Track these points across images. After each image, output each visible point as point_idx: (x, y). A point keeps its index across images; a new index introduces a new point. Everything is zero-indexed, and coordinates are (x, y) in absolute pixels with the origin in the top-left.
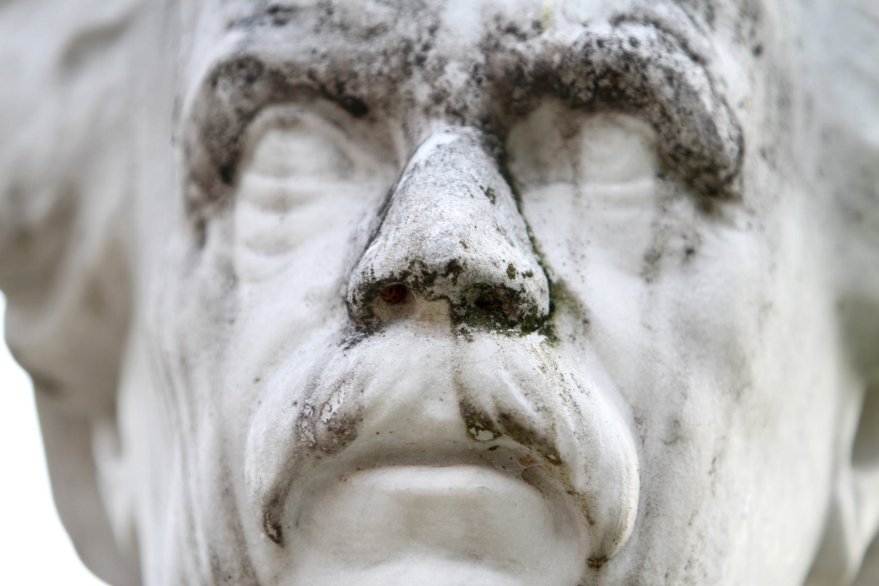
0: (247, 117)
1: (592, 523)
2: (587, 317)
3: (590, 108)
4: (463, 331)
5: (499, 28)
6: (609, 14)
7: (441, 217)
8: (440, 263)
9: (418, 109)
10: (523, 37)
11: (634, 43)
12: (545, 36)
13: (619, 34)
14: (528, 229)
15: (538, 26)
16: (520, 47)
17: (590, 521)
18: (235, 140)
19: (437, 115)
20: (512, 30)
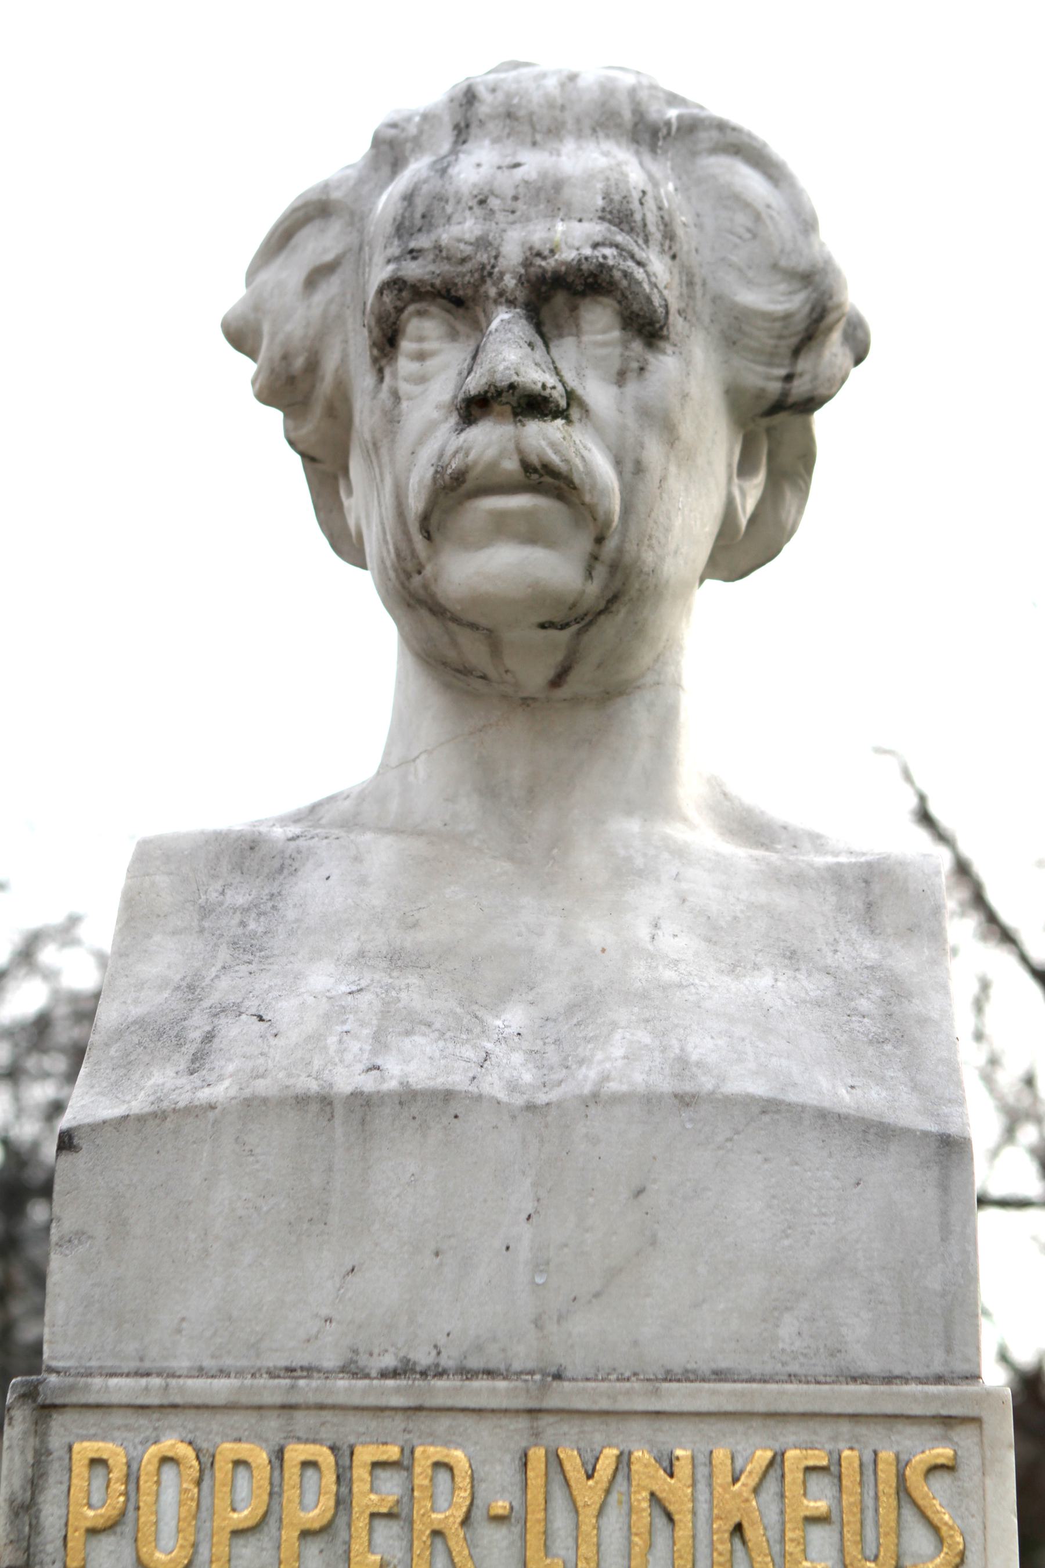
1: (595, 519)
6: (590, 242)
10: (544, 258)
11: (605, 257)
12: (557, 257)
13: (596, 253)
15: (552, 252)
16: (543, 263)
18: (394, 323)
20: (539, 254)
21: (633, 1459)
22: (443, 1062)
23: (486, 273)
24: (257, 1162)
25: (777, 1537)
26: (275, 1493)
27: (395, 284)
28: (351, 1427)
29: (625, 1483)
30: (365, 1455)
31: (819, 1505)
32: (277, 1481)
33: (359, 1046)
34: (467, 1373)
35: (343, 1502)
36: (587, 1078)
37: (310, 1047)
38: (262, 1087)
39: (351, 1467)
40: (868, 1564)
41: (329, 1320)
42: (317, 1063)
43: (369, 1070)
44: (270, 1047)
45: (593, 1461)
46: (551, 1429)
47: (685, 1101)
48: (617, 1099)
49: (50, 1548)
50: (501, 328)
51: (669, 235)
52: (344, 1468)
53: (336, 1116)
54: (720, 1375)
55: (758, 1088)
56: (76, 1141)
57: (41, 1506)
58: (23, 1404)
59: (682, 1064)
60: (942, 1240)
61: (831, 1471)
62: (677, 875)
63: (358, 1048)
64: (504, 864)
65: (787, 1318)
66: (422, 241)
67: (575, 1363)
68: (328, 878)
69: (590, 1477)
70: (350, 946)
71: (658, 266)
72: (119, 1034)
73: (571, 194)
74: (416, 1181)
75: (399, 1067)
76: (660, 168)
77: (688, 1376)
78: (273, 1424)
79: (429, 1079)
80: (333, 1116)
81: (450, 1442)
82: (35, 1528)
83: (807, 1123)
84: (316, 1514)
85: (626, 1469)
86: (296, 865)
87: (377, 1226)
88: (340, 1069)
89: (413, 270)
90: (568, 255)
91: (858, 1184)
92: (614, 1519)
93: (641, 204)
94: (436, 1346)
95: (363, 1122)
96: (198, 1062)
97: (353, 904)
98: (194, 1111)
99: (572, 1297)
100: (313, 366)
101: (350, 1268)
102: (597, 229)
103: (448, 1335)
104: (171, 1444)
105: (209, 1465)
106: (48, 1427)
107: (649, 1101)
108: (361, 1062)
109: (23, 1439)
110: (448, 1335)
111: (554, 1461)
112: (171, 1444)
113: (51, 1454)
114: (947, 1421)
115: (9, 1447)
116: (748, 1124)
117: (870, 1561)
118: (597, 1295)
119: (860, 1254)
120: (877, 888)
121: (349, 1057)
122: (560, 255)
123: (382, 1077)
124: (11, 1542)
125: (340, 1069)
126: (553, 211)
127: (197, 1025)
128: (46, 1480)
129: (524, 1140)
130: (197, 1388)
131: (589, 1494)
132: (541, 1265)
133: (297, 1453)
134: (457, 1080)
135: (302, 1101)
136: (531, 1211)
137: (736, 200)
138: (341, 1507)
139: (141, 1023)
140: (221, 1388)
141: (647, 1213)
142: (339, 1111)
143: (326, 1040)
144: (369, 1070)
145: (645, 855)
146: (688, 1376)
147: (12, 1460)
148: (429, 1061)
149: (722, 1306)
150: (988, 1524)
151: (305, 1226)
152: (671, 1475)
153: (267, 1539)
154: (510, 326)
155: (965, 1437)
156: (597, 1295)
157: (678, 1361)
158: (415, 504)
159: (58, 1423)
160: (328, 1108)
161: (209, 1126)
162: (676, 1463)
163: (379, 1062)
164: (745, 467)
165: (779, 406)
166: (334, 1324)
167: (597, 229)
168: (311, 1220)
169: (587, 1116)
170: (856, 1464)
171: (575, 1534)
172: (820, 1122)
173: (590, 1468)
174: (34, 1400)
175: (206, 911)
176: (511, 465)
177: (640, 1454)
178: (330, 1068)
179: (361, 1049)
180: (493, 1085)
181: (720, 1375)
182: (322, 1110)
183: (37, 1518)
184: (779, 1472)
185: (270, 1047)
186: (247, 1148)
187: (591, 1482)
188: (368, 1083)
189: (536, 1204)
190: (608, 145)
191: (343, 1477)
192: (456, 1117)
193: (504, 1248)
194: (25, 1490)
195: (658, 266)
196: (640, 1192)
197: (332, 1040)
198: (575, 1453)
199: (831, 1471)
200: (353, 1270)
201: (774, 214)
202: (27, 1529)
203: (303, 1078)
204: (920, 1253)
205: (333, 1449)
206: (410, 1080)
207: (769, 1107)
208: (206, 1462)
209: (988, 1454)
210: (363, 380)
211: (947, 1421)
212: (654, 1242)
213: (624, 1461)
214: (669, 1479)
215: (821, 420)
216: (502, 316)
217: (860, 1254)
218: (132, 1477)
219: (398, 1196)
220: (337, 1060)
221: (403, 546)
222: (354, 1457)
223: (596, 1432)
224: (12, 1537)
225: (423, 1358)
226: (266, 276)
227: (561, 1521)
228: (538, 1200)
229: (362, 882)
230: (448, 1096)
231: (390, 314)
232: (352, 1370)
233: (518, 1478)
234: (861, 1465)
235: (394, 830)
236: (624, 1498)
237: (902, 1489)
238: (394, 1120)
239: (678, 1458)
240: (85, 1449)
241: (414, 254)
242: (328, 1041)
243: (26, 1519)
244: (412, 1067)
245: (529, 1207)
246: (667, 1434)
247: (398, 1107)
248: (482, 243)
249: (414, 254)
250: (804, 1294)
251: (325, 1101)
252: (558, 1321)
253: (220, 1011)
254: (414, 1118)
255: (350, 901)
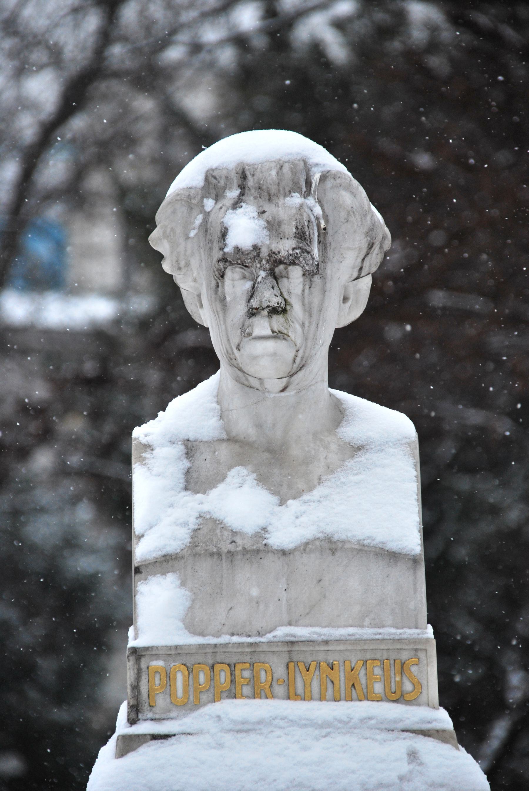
0: (225, 268)
1: (296, 346)
2: (292, 305)
3: (290, 265)
4: (270, 315)
5: (271, 252)
6: (292, 248)
7: (265, 297)
8: (266, 453)
9: (258, 268)
10: (276, 254)
11: (297, 254)
12: (280, 254)
13: (294, 252)
14: (280, 290)
15: (279, 252)
16: (276, 256)
17: (236, 732)
18: (224, 272)
19: (261, 269)
20: (274, 253)
21: (321, 665)
22: (255, 539)
24: (199, 575)
25: (365, 687)
29: (319, 672)
32: (212, 676)
33: (227, 533)
37: (211, 534)
39: (235, 671)
40: (393, 694)
41: (224, 624)
42: (215, 540)
43: (232, 543)
44: (198, 534)
45: (308, 666)
49: (144, 699)
50: (262, 281)
52: (232, 671)
53: (223, 559)
56: (141, 570)
57: (140, 686)
58: (132, 655)
60: (414, 593)
62: (326, 456)
64: (266, 454)
65: (367, 619)
68: (205, 460)
69: (308, 671)
74: (249, 579)
75: (241, 541)
79: (251, 546)
80: (222, 560)
82: (139, 693)
83: (371, 557)
85: (319, 668)
86: (193, 452)
87: (238, 594)
88: (222, 543)
91: (388, 576)
93: (308, 227)
94: (258, 632)
95: (232, 561)
97: (216, 472)
99: (300, 615)
101: (230, 608)
103: (262, 628)
105: (191, 672)
106: (140, 662)
108: (229, 539)
109: (133, 666)
110: (262, 628)
113: (142, 670)
115: (129, 668)
116: (353, 558)
117: (393, 693)
118: (308, 614)
119: (389, 599)
121: (225, 538)
122: (281, 254)
123: (236, 545)
124: (132, 697)
125: (222, 543)
126: (278, 235)
128: (141, 678)
129: (283, 565)
136: (286, 588)
138: (232, 683)
141: (322, 588)
142: (224, 557)
143: (216, 531)
144: (232, 543)
145: (315, 449)
147: (130, 673)
148: (250, 539)
149: (346, 616)
150: (429, 681)
151: (216, 595)
152: (332, 669)
153: (210, 693)
154: (266, 280)
156: (308, 614)
160: (220, 557)
161: (183, 564)
162: (334, 666)
163: (234, 539)
166: (226, 626)
168: (217, 593)
169: (302, 557)
170: (389, 664)
171: (304, 688)
172: (376, 556)
173: (308, 668)
174: (136, 654)
177: (323, 663)
178: (219, 542)
179: (228, 534)
182: (218, 558)
183: (139, 690)
184: (365, 667)
185: (198, 534)
186: (196, 571)
187: (308, 673)
189: (287, 586)
192: (261, 558)
193: (278, 600)
194: (135, 682)
196: (320, 581)
197: (218, 531)
198: (303, 664)
200: (231, 609)
201: (354, 210)
202: (137, 693)
203: (211, 546)
204: (407, 597)
205: (229, 665)
206: (245, 546)
209: (429, 660)
212: (325, 597)
214: (332, 671)
217: (389, 599)
219: (244, 584)
220: (221, 539)
221: (228, 346)
222: (236, 668)
224: (132, 696)
228: (288, 585)
229: (218, 462)
231: (222, 269)
233: (286, 672)
234: (390, 664)
236: (318, 677)
238: (241, 560)
239: (334, 664)
242: (217, 532)
243: (136, 690)
244: (245, 541)
245: (285, 587)
247: (242, 556)
250: (372, 611)
252: (296, 622)
254: (248, 559)
255: (215, 471)
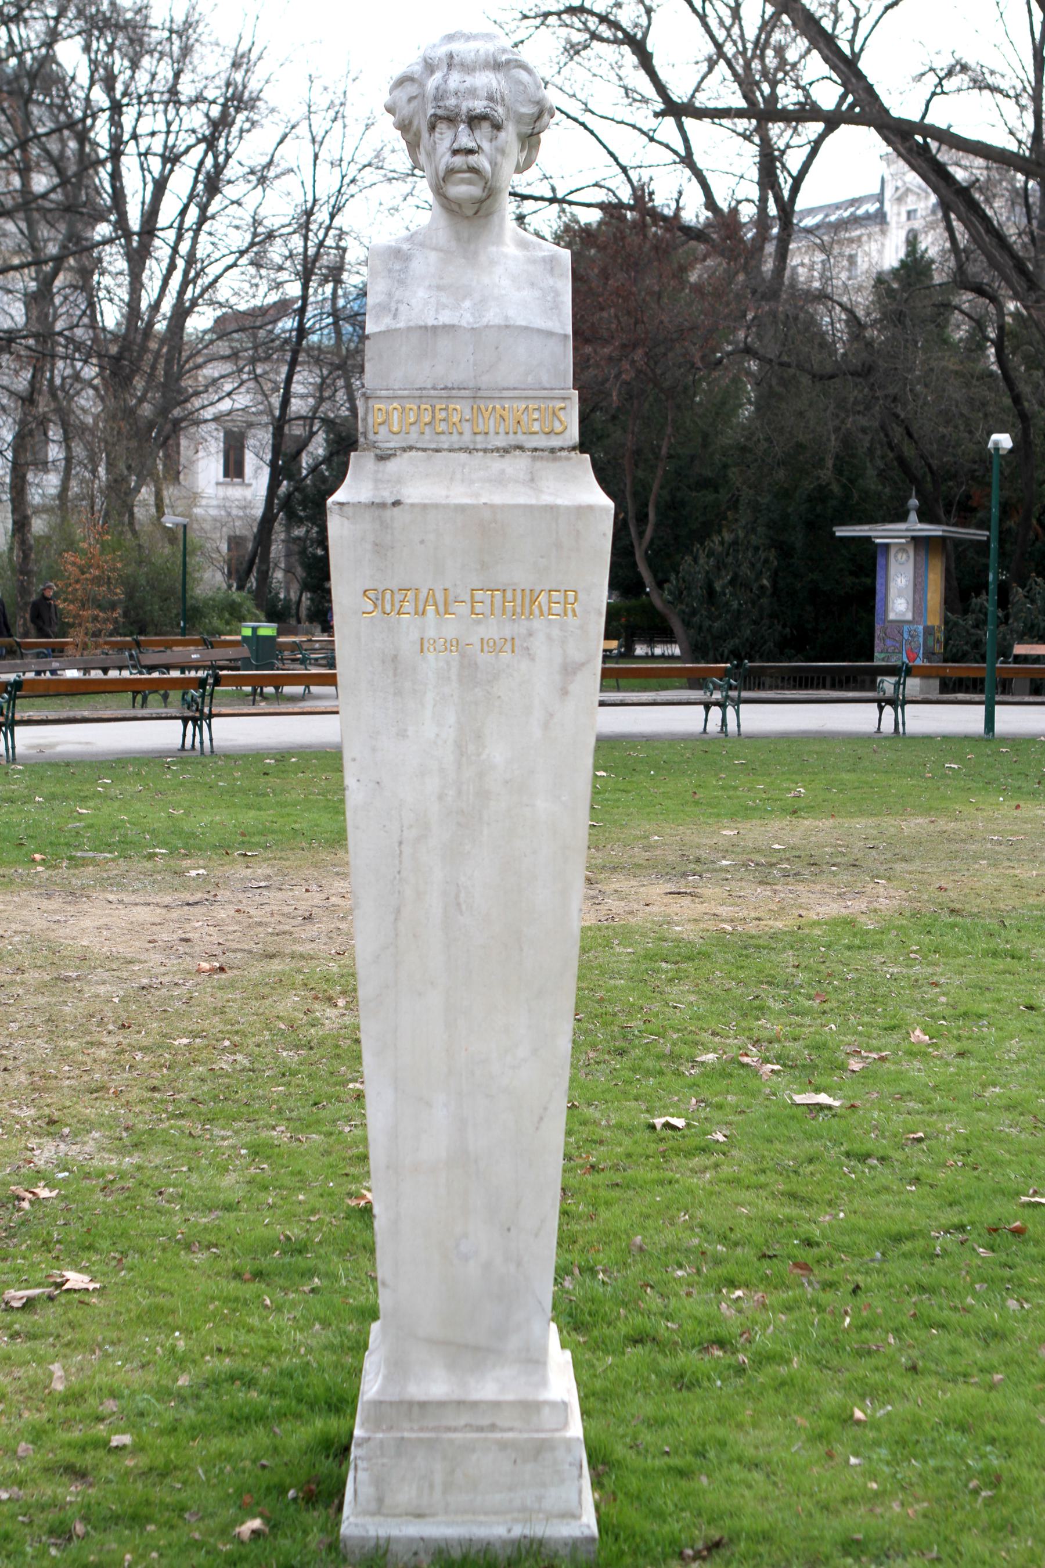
23: (457, 114)
26: (419, 415)
27: (435, 115)
28: (434, 401)
30: (438, 407)
31: (536, 416)
34: (459, 389)
35: (433, 417)
36: (484, 321)
38: (412, 324)
46: (478, 401)
47: (507, 327)
48: (492, 326)
51: (503, 99)
54: (515, 389)
55: (524, 323)
59: (506, 318)
61: (538, 409)
63: (432, 313)
66: (441, 104)
67: (483, 386)
70: (427, 283)
71: (500, 110)
72: (374, 307)
73: (479, 92)
76: (500, 76)
77: (508, 389)
78: (417, 401)
81: (931, 808)
84: (427, 419)
89: (440, 112)
90: (478, 111)
92: (492, 421)
96: (395, 316)
98: (396, 330)
100: (411, 123)
102: (485, 103)
104: (395, 405)
107: (499, 327)
111: (479, 408)
112: (395, 405)
114: (564, 399)
120: (276, 1389)
127: (393, 306)
130: (400, 393)
131: (486, 415)
132: (475, 365)
133: (423, 407)
134: (455, 322)
135: (421, 327)
137: (520, 82)
139: (379, 304)
140: (406, 393)
146: (508, 389)
155: (568, 402)
157: (506, 385)
158: (441, 174)
159: (371, 402)
164: (522, 150)
165: (531, 135)
167: (485, 103)
175: (390, 271)
176: (465, 167)
180: (464, 323)
181: (515, 389)
188: (435, 323)
190: (488, 73)
191: (433, 412)
195: (500, 110)
199: (538, 409)
207: (526, 328)
208: (404, 409)
210: (425, 134)
211: (564, 399)
213: (494, 408)
215: (542, 135)
216: (462, 126)
218: (387, 413)
223: (488, 401)
225: (450, 385)
226: (395, 93)
227: (481, 420)
230: (453, 326)
232: (434, 388)
235: (435, 249)
237: (554, 413)
240: (377, 406)
241: (439, 107)
246: (503, 402)
248: (457, 106)
249: (439, 107)
251: (426, 327)
253: (398, 302)
